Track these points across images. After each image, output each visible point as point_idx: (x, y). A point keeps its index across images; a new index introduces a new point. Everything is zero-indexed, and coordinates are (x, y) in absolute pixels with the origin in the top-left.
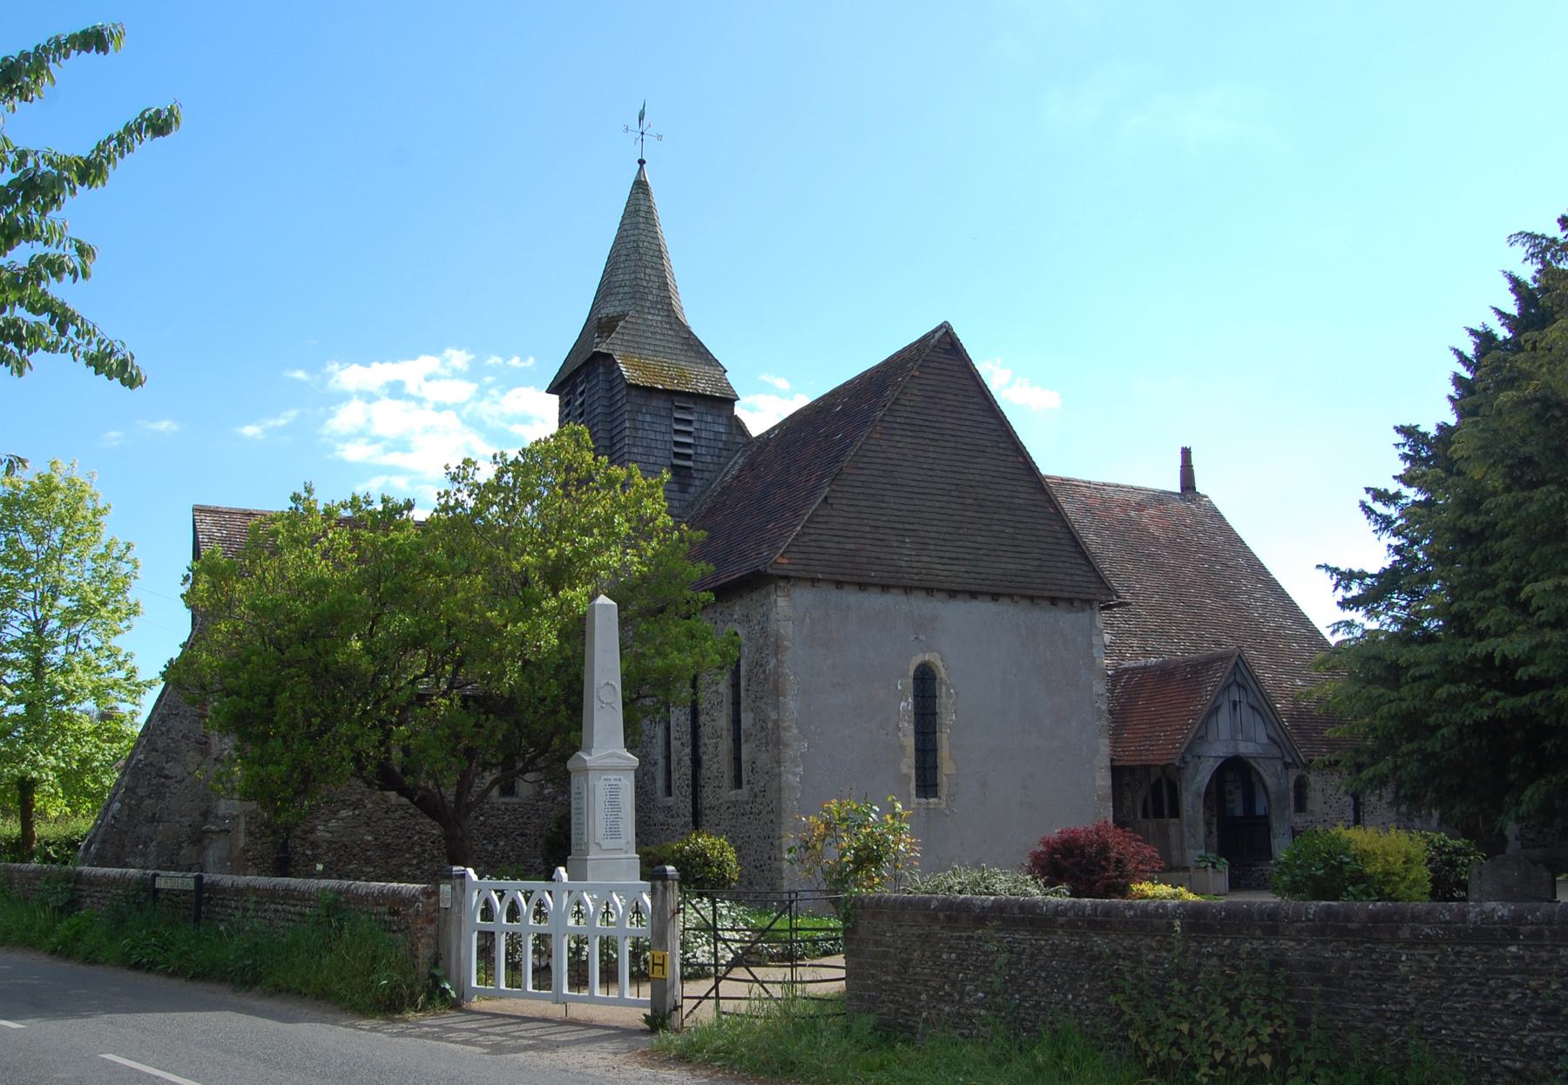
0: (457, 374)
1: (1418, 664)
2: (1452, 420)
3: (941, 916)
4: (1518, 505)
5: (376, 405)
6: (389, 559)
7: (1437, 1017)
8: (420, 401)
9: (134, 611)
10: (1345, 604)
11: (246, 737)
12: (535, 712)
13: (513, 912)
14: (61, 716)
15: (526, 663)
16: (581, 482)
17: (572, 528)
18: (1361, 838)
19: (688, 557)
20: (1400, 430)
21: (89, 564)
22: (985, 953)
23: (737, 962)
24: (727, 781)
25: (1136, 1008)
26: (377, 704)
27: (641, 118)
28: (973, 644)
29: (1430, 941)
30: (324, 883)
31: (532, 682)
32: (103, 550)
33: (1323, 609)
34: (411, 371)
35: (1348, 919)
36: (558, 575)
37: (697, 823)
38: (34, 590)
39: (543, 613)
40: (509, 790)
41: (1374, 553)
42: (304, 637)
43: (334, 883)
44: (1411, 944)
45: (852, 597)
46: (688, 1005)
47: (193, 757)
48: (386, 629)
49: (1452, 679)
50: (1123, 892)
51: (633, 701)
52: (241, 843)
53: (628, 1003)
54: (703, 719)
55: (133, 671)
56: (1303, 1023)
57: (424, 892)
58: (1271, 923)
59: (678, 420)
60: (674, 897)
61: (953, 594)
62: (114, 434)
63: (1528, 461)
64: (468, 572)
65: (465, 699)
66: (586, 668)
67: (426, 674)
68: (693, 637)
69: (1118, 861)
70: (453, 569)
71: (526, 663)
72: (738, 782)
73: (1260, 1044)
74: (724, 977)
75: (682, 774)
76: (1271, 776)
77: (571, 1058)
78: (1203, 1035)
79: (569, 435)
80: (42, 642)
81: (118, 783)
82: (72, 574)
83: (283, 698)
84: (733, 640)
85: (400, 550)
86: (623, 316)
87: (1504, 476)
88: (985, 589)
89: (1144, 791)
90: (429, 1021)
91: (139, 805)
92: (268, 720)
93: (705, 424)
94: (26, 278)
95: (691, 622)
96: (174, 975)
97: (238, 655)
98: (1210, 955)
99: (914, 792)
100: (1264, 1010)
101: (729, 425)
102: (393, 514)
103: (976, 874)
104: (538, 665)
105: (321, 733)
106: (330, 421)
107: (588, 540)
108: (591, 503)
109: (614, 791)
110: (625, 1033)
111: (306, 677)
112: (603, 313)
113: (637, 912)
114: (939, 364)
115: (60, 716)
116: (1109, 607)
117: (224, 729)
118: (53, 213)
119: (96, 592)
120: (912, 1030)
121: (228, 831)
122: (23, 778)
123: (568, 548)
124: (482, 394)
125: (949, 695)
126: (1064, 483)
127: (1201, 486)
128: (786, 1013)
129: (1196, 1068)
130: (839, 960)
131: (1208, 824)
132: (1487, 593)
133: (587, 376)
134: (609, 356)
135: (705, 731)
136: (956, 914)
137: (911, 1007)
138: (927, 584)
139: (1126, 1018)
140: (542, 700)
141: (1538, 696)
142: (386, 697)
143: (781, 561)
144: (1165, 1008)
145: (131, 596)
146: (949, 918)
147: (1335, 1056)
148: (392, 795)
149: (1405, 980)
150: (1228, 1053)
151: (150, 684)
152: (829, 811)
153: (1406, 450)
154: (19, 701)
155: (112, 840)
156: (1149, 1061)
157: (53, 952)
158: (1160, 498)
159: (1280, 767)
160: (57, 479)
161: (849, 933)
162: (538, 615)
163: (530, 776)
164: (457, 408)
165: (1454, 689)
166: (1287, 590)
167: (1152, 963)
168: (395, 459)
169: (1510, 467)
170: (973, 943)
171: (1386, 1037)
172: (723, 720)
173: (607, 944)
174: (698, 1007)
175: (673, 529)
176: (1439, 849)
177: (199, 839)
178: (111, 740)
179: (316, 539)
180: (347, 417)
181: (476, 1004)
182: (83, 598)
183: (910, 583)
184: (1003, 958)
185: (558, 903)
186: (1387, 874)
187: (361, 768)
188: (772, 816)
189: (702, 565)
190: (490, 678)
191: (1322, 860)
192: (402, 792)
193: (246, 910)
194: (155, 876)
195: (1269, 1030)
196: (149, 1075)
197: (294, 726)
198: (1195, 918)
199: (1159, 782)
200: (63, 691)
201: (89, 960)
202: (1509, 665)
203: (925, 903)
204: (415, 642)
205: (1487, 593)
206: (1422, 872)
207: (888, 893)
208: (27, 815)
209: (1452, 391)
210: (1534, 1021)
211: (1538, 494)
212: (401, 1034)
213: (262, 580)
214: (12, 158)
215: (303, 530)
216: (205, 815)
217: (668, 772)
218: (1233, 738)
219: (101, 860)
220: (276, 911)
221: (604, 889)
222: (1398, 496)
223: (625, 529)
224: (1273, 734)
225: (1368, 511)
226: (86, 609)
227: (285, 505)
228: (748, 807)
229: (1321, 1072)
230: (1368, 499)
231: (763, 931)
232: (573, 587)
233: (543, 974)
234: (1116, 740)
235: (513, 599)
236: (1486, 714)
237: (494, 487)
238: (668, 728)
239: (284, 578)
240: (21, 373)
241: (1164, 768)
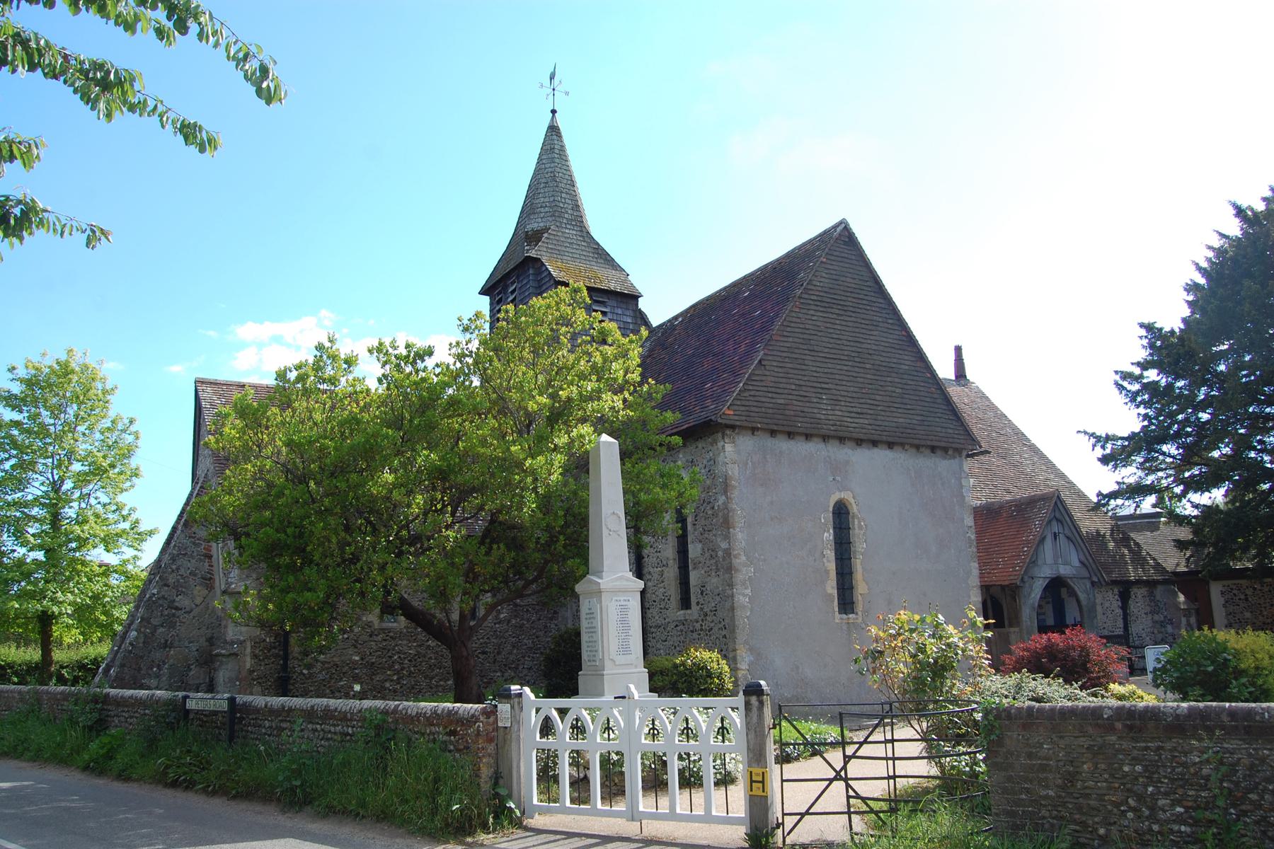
3: (1119, 725)
14: (74, 560)
20: (1142, 325)
21: (98, 436)
22: (1184, 765)
27: (552, 77)
28: (875, 481)
30: (367, 703)
32: (109, 424)
36: (559, 415)
41: (1127, 420)
43: (379, 704)
45: (783, 444)
47: (199, 591)
52: (248, 665)
54: (645, 552)
55: (137, 522)
61: (859, 442)
72: (685, 603)
80: (59, 499)
81: (132, 616)
82: (85, 442)
86: (546, 229)
88: (884, 438)
91: (153, 634)
96: (214, 793)
99: (836, 609)
101: (635, 317)
109: (624, 610)
112: (529, 228)
115: (74, 560)
116: (972, 456)
121: (236, 655)
122: (44, 613)
125: (860, 528)
127: (970, 374)
133: (518, 277)
138: (841, 434)
143: (728, 413)
145: (134, 462)
146: (1131, 728)
154: (41, 547)
155: (133, 662)
157: (86, 768)
160: (73, 365)
166: (1045, 452)
177: (208, 660)
181: (538, 821)
183: (828, 433)
185: (629, 720)
186: (1257, 668)
188: (724, 632)
194: (185, 697)
200: (78, 539)
201: (123, 776)
208: (46, 643)
216: (211, 641)
219: (120, 683)
220: (315, 730)
221: (622, 705)
224: (1083, 559)
225: (1121, 388)
226: (97, 472)
228: (698, 626)
230: (1117, 378)
233: (580, 785)
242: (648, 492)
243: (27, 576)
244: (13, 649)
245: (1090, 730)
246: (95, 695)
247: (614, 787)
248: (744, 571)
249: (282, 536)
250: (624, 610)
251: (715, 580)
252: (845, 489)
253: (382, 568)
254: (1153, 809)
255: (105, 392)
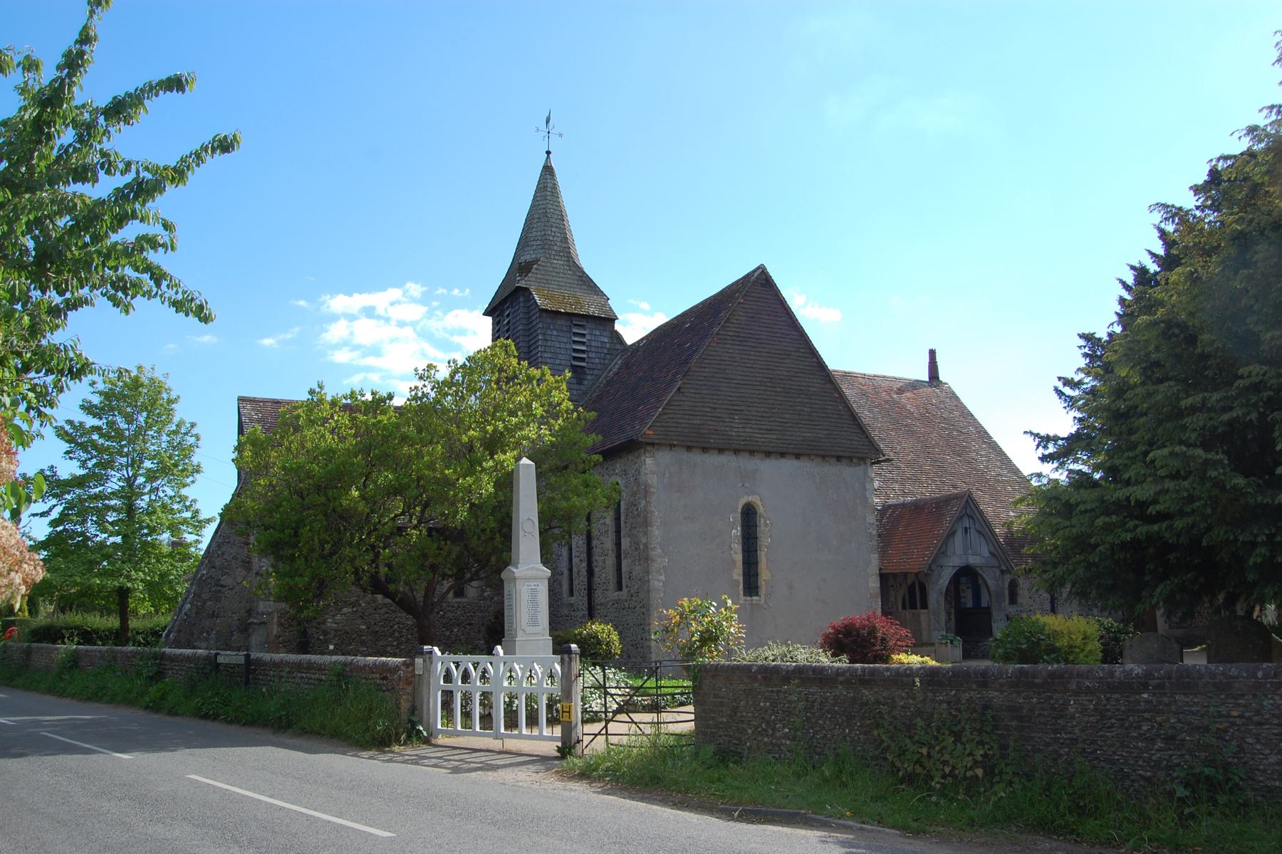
0: (413, 300)
1: (1084, 502)
2: (1118, 329)
4: (1149, 395)
5: (356, 323)
6: (378, 434)
7: (1094, 742)
8: (387, 320)
9: (197, 470)
10: (1044, 459)
11: (279, 558)
12: (479, 538)
13: (466, 677)
14: (146, 543)
15: (472, 505)
16: (509, 380)
17: (503, 411)
18: (1052, 622)
19: (583, 431)
20: (1082, 336)
21: (165, 438)
22: (789, 702)
23: (619, 711)
24: (612, 586)
25: (892, 738)
26: (369, 535)
27: (548, 122)
29: (1089, 691)
30: (334, 658)
31: (477, 518)
33: (1027, 460)
34: (379, 300)
35: (1034, 676)
36: (494, 444)
37: (591, 615)
38: (127, 455)
39: (484, 470)
40: (460, 593)
41: (1064, 424)
42: (318, 489)
43: (341, 658)
44: (1076, 693)
45: (697, 457)
46: (587, 739)
47: (240, 572)
48: (375, 482)
49: (1107, 513)
50: (886, 660)
51: (546, 530)
52: (275, 632)
53: (546, 740)
54: (594, 542)
55: (197, 512)
56: (1004, 747)
57: (404, 663)
58: (983, 680)
59: (576, 334)
60: (576, 666)
61: (768, 454)
62: (171, 346)
63: (1157, 364)
64: (431, 442)
65: (430, 530)
66: (514, 509)
67: (403, 513)
68: (587, 486)
69: (883, 639)
70: (421, 440)
71: (472, 505)
72: (620, 588)
73: (976, 762)
74: (612, 720)
75: (580, 581)
76: (991, 579)
77: (507, 775)
78: (936, 756)
79: (501, 347)
80: (133, 493)
81: (188, 591)
83: (305, 531)
84: (615, 488)
85: (385, 428)
87: (1141, 375)
89: (904, 592)
90: (409, 751)
92: (295, 546)
93: (591, 334)
94: (133, 249)
95: (586, 476)
96: (231, 722)
97: (272, 501)
98: (941, 702)
100: (978, 739)
101: (611, 337)
102: (379, 403)
103: (785, 649)
104: (479, 507)
105: (331, 555)
106: (324, 335)
107: (514, 420)
108: (516, 394)
109: (534, 593)
110: (543, 759)
111: (320, 517)
113: (551, 676)
114: (757, 293)
116: (879, 462)
117: (263, 553)
118: (149, 204)
119: (170, 458)
120: (740, 755)
121: (265, 623)
122: (121, 588)
123: (501, 425)
124: (430, 314)
125: (766, 525)
126: (846, 375)
128: (654, 745)
129: (932, 778)
130: (691, 708)
131: (949, 614)
132: (1131, 454)
134: (527, 289)
135: (596, 551)
136: (769, 674)
137: (739, 739)
139: (885, 745)
140: (483, 530)
141: (1164, 525)
142: (376, 529)
143: (648, 432)
144: (911, 737)
147: (1026, 769)
148: (379, 597)
149: (1073, 717)
150: (954, 768)
151: (209, 521)
152: (682, 606)
153: (1086, 350)
155: (186, 632)
156: (901, 774)
157: (147, 708)
158: (915, 385)
159: (998, 573)
161: (696, 690)
162: (481, 472)
163: (475, 584)
164: (413, 324)
165: (1107, 519)
167: (903, 707)
168: (370, 361)
169: (1145, 369)
170: (782, 696)
171: (1061, 756)
172: (609, 543)
173: (531, 699)
174: (593, 741)
175: (573, 411)
176: (1108, 630)
177: (245, 628)
178: (182, 561)
179: (325, 420)
180: (337, 332)
181: (441, 740)
182: (161, 462)
184: (801, 705)
185: (496, 671)
186: (1071, 647)
187: (359, 579)
189: (594, 436)
190: (447, 516)
191: (1026, 637)
192: (387, 594)
193: (281, 677)
194: (216, 654)
195: (982, 752)
196: (221, 789)
197: (312, 550)
198: (930, 676)
199: (913, 584)
200: (148, 527)
201: (172, 713)
202: (1142, 505)
203: (748, 668)
204: (394, 491)
205: (1131, 454)
206: (1095, 646)
207: (723, 662)
208: (124, 614)
209: (1118, 309)
210: (1160, 744)
211: (1162, 387)
212: (390, 761)
213: (289, 449)
214: (121, 166)
215: (318, 414)
216: (250, 612)
217: (571, 580)
218: (965, 553)
221: (526, 663)
222: (1080, 383)
223: (539, 411)
224: (992, 549)
225: (1060, 393)
226: (164, 470)
227: (305, 396)
229: (1016, 780)
230: (1060, 385)
231: (637, 689)
232: (504, 452)
233: (487, 720)
234: (883, 554)
235: (463, 461)
236: (1128, 536)
237: (449, 383)
238: (570, 549)
239: (303, 447)
240: (127, 312)
241: (917, 574)
242: (568, 499)
243: (107, 557)
244: (98, 618)
245: (745, 680)
246: (155, 653)
247: (512, 722)
248: (660, 560)
249: (282, 536)
250: (534, 593)
251: (638, 568)
252: (752, 493)
253: (352, 560)
254: (774, 730)
255: (170, 401)
